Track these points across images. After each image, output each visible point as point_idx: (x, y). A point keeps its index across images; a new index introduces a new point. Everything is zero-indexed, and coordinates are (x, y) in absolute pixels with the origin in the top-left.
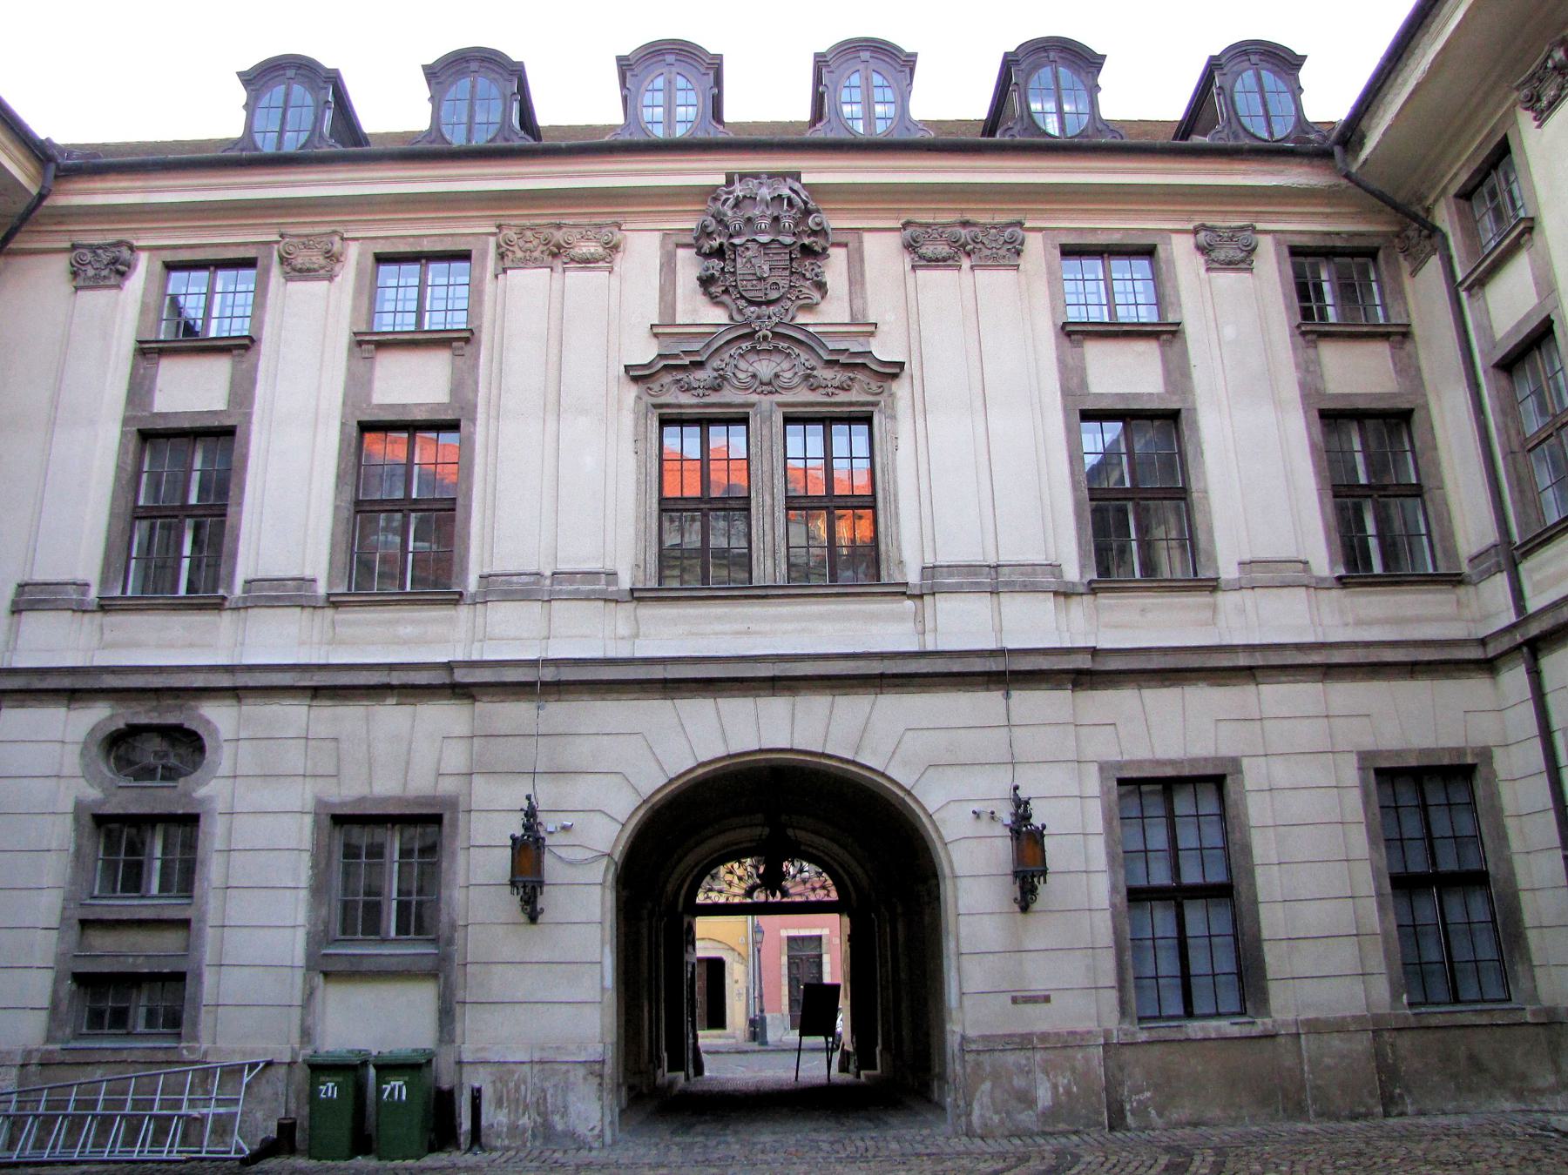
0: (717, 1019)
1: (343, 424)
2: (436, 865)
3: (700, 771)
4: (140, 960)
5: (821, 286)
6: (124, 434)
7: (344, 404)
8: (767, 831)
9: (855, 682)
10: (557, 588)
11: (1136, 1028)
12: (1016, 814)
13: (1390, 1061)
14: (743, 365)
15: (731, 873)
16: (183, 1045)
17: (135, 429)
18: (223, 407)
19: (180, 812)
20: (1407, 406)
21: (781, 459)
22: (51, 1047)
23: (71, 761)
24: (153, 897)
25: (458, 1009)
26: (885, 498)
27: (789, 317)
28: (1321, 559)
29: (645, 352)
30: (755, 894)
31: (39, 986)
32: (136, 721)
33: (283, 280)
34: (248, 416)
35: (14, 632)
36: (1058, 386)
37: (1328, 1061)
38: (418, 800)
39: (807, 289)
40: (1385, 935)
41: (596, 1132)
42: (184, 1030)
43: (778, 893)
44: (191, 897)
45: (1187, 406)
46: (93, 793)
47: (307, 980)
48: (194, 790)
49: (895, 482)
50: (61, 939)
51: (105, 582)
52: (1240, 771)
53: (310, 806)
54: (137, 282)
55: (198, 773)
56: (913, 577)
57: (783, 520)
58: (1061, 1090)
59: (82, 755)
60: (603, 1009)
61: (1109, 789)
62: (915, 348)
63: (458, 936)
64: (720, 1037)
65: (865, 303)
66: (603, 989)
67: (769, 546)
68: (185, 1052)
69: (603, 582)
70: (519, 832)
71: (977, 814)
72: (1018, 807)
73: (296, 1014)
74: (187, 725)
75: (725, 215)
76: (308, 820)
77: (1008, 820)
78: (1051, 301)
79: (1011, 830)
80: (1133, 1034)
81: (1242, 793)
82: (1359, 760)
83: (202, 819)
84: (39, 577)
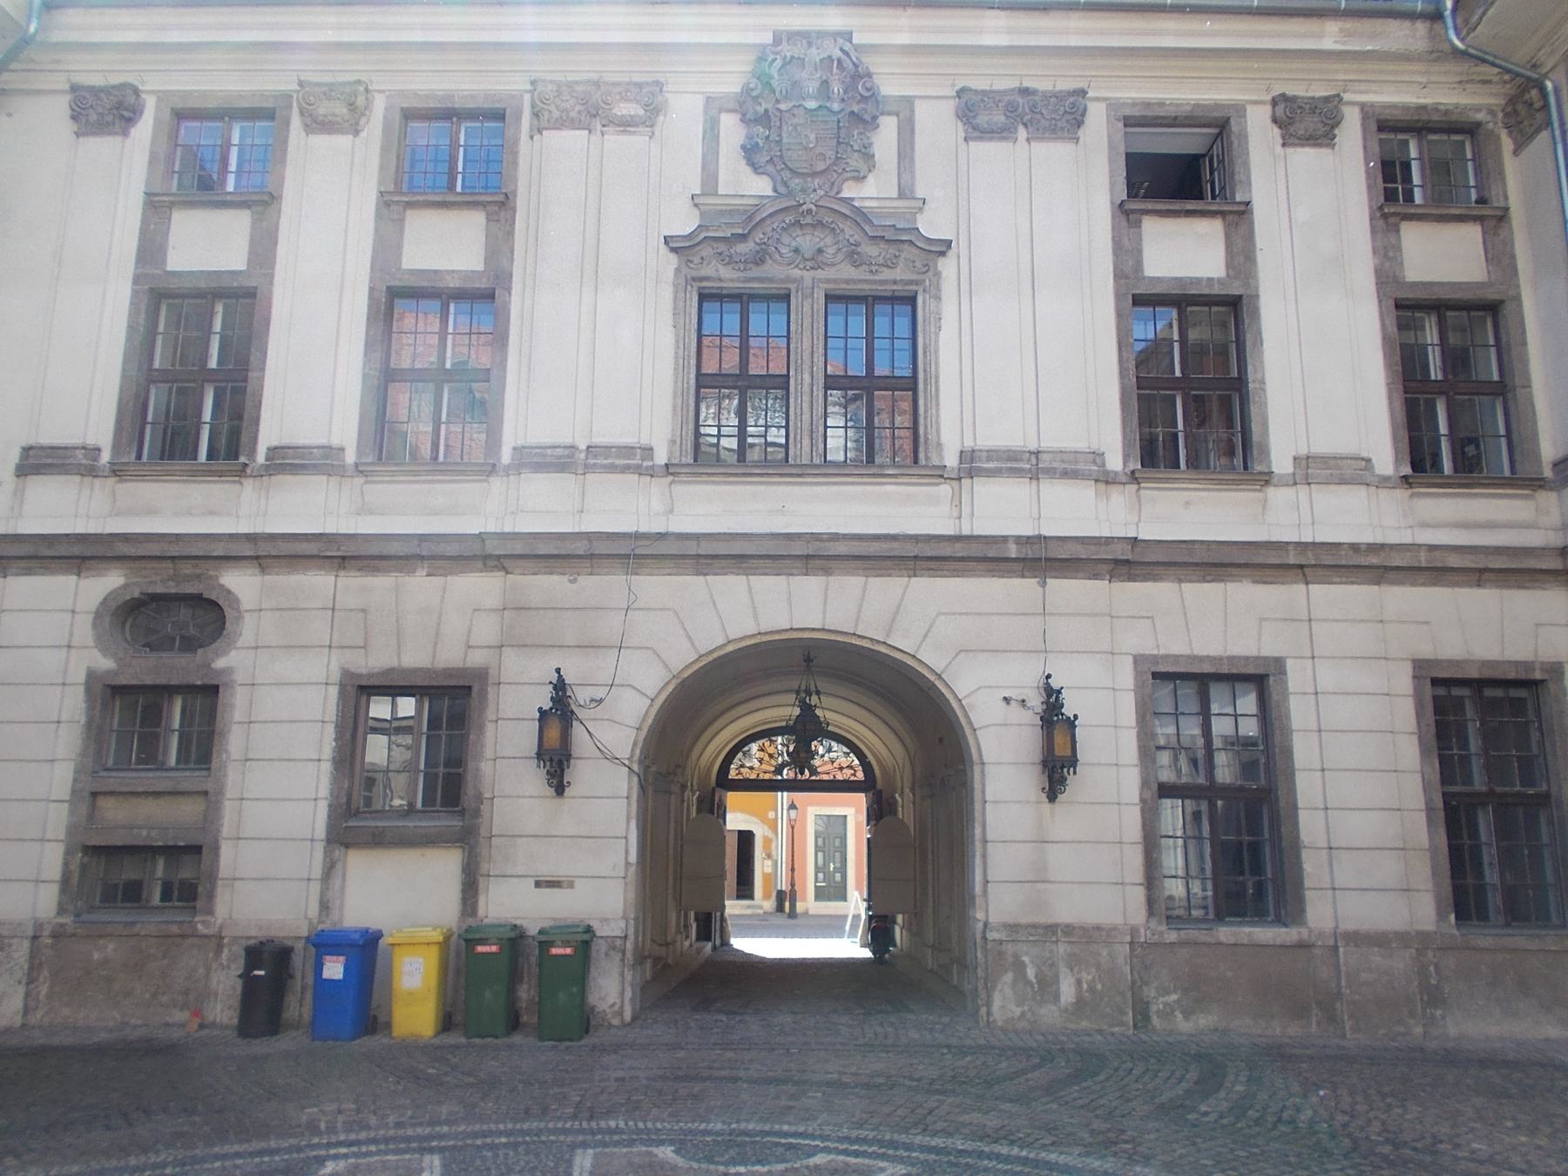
0: (745, 888)
1: (372, 289)
2: (464, 738)
3: (730, 648)
4: (154, 833)
5: (869, 157)
6: (135, 293)
7: (372, 269)
8: (797, 711)
9: (889, 563)
10: (592, 461)
11: (1164, 928)
12: (1047, 703)
13: (1433, 982)
14: (786, 239)
15: (762, 750)
16: (197, 919)
17: (146, 287)
18: (244, 268)
19: (199, 683)
20: (1497, 297)
21: (822, 338)
22: (61, 920)
23: (84, 630)
24: (172, 769)
25: (482, 881)
26: (925, 380)
27: (835, 190)
28: (1385, 456)
29: (684, 223)
30: (785, 771)
31: (52, 860)
32: (150, 590)
33: (304, 134)
34: (270, 277)
35: (19, 494)
36: (1111, 269)
37: (1364, 976)
38: (449, 672)
39: (855, 161)
40: (1433, 850)
41: (616, 1008)
42: (199, 904)
43: (806, 771)
44: (209, 769)
45: (1249, 292)
46: (105, 664)
47: (328, 853)
48: (213, 661)
49: (937, 364)
50: (72, 812)
51: (116, 447)
52: (1284, 673)
53: (336, 676)
54: (144, 130)
55: (218, 643)
56: (951, 460)
57: (821, 400)
58: (1085, 986)
59: (95, 626)
60: (626, 884)
61: (1143, 682)
62: (963, 227)
63: (485, 808)
64: (749, 907)
65: (913, 177)
66: (627, 864)
67: (806, 426)
68: (199, 926)
69: (638, 457)
70: (547, 705)
71: (1007, 700)
72: (1049, 696)
73: (316, 888)
74: (206, 595)
75: (771, 77)
76: (334, 692)
77: (1040, 709)
78: (1111, 177)
79: (1042, 718)
80: (1161, 933)
81: (1285, 695)
82: (1414, 668)
83: (221, 690)
84: (46, 439)
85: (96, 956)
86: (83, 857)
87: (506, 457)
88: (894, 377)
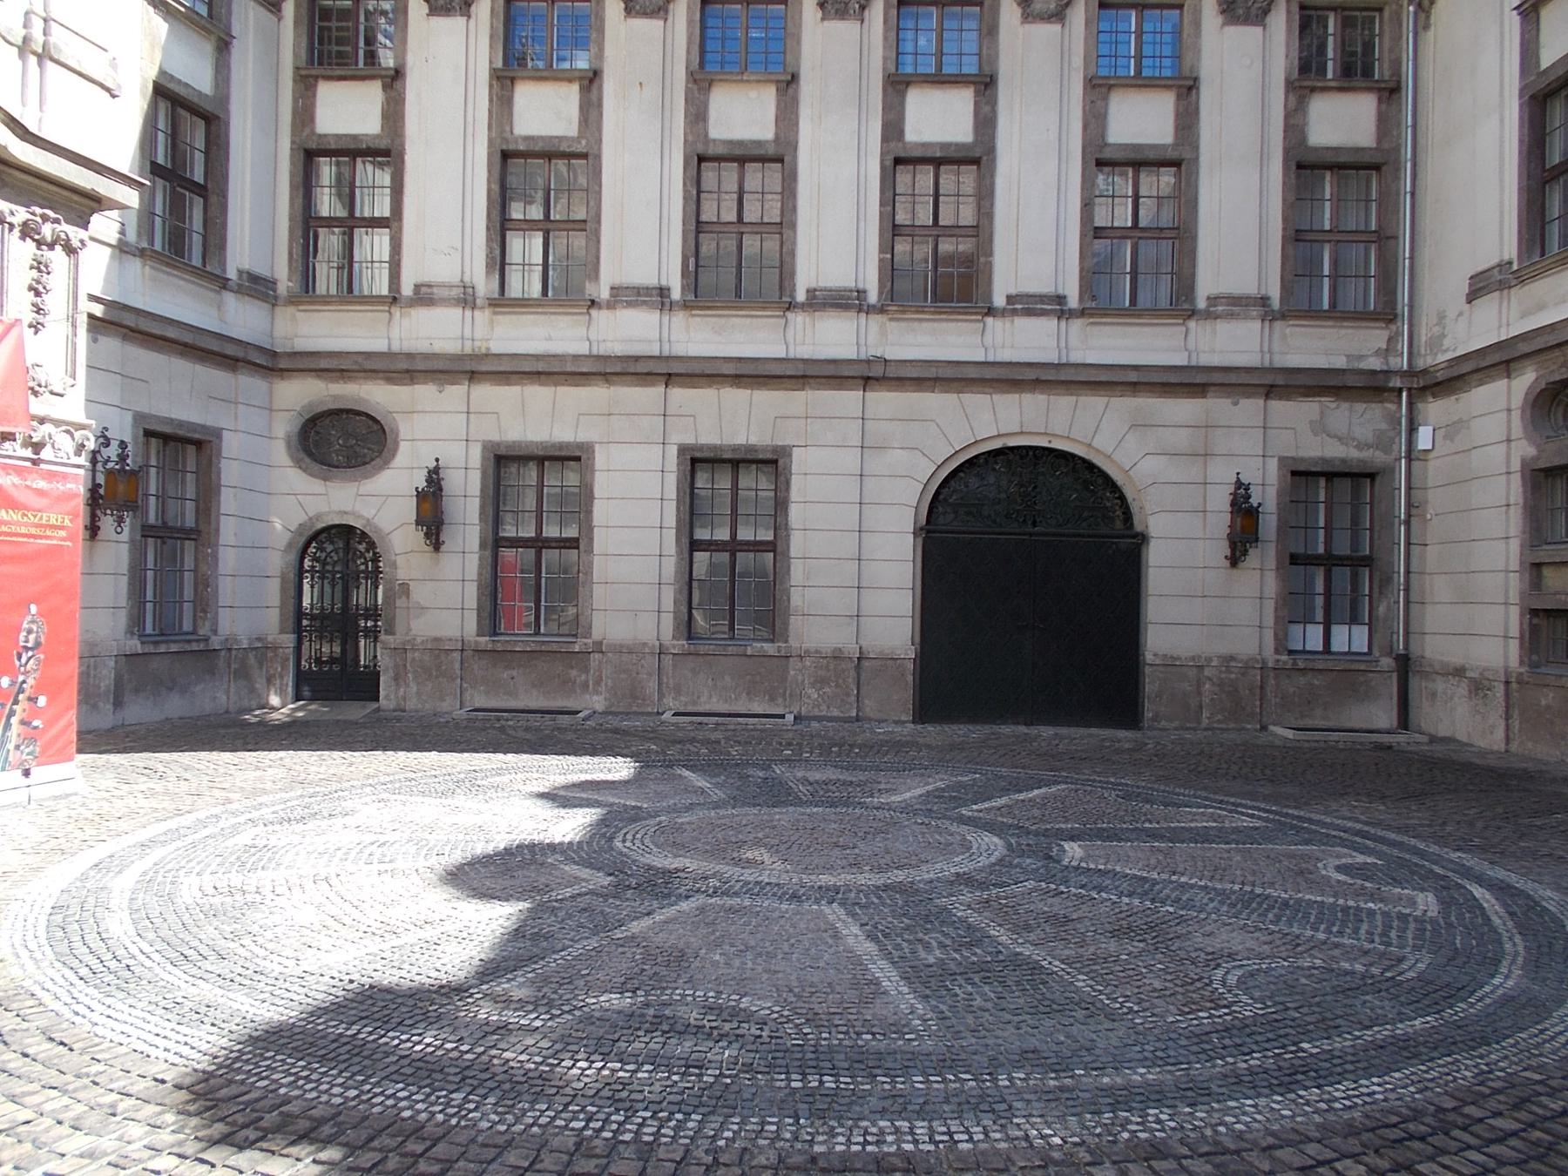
76: (1516, 480)
85: (1543, 702)
86: (1530, 619)
87: (801, 296)
88: (762, 223)
